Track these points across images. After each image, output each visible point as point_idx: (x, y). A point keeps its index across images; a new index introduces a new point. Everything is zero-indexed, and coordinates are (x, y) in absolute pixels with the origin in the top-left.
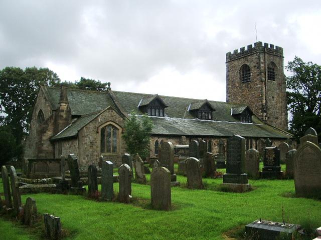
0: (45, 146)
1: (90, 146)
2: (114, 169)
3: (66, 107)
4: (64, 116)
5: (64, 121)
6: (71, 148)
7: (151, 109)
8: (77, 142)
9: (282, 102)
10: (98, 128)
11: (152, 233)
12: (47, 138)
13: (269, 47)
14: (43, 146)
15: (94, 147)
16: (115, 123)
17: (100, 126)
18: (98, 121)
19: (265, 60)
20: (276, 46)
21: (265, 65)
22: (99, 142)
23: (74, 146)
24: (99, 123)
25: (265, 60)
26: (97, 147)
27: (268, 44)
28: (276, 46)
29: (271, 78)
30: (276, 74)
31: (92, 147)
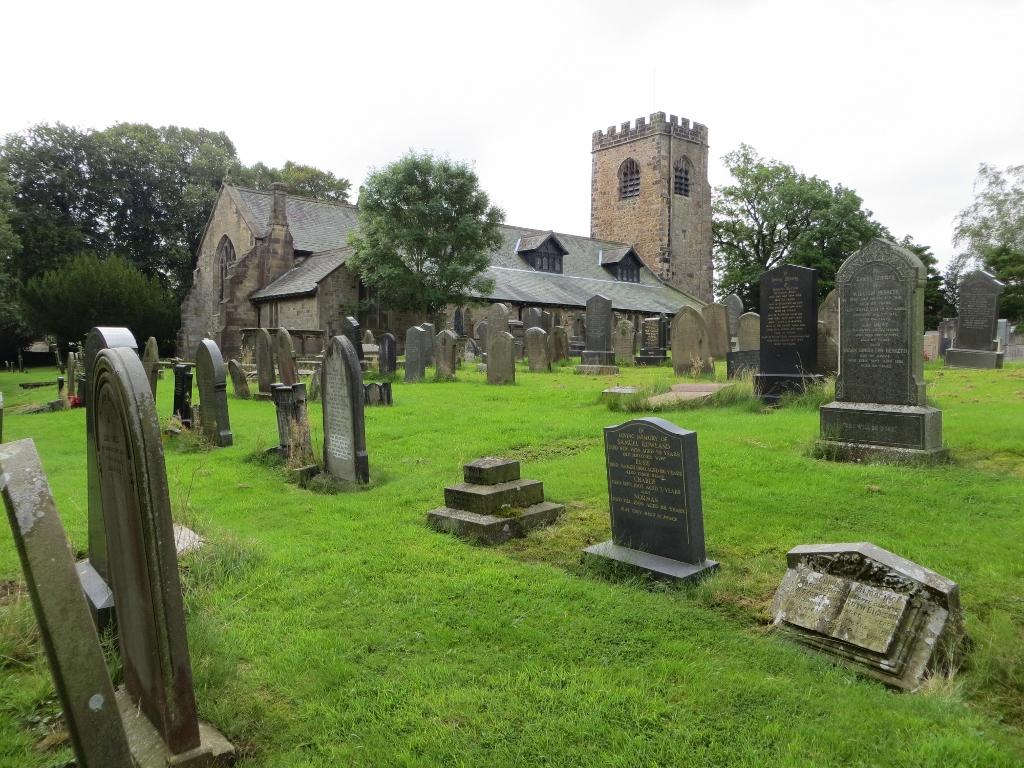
6: (301, 315)
20: (695, 123)
23: (308, 311)
28: (695, 123)
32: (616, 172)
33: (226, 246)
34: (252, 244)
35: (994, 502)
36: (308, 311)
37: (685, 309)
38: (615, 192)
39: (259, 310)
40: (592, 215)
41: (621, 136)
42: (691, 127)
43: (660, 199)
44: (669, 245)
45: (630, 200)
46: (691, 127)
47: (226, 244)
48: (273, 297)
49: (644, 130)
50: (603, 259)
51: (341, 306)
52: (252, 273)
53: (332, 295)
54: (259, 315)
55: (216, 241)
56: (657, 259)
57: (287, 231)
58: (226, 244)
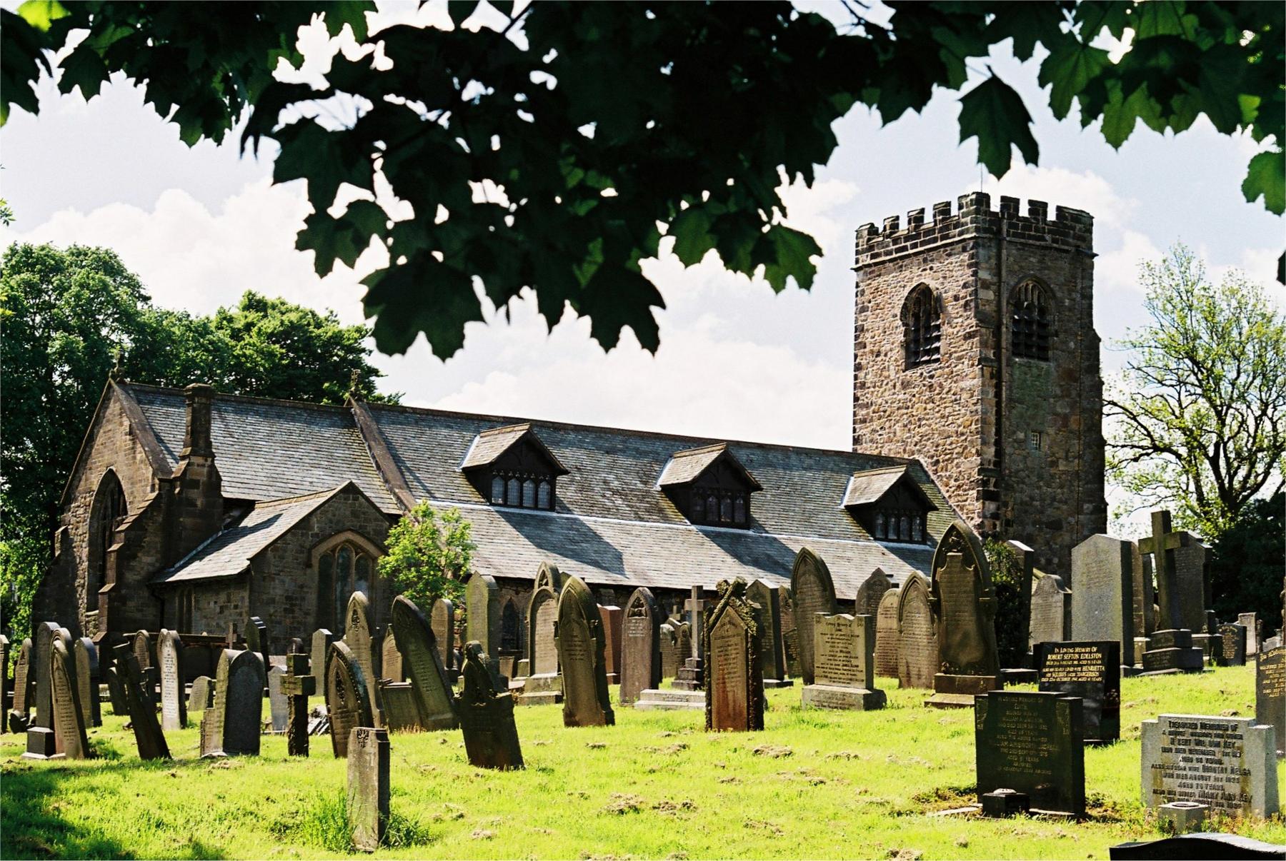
0: (131, 604)
1: (285, 610)
2: (1229, 40)
3: (205, 470)
4: (199, 503)
5: (199, 520)
6: (226, 612)
7: (506, 479)
8: (246, 594)
9: (1079, 457)
10: (310, 551)
11: (1068, 396)
12: (138, 577)
13: (1024, 211)
14: (124, 604)
15: (298, 613)
16: (362, 535)
17: (315, 546)
18: (312, 529)
19: (999, 274)
20: (1059, 209)
21: (998, 294)
22: (312, 598)
23: (236, 607)
24: (317, 535)
25: (999, 274)
26: (307, 614)
27: (1016, 202)
28: (1059, 209)
29: (1028, 347)
30: (1052, 329)
31: (293, 612)
32: (898, 311)
33: (111, 486)
34: (153, 490)
35: (669, 735)
36: (236, 607)
37: (739, 589)
38: (897, 354)
39: (163, 603)
40: (856, 399)
41: (907, 238)
42: (1052, 216)
43: (977, 369)
44: (996, 464)
45: (924, 370)
46: (1052, 216)
47: (112, 485)
48: (1123, 602)
49: (947, 228)
50: (851, 499)
51: (288, 598)
52: (153, 538)
53: (273, 580)
54: (162, 613)
55: (94, 479)
56: (974, 493)
57: (213, 467)
58: (112, 485)
